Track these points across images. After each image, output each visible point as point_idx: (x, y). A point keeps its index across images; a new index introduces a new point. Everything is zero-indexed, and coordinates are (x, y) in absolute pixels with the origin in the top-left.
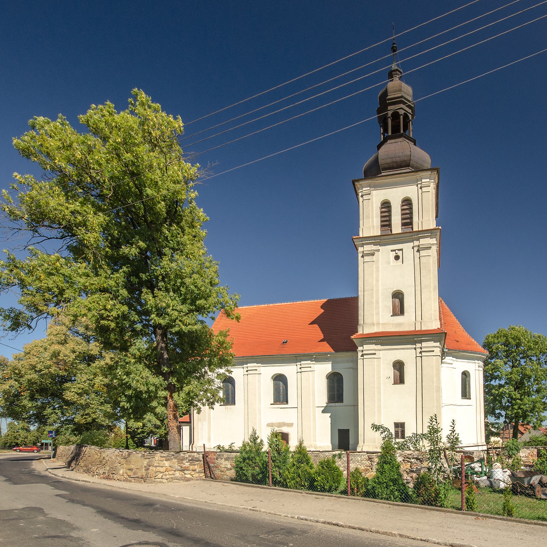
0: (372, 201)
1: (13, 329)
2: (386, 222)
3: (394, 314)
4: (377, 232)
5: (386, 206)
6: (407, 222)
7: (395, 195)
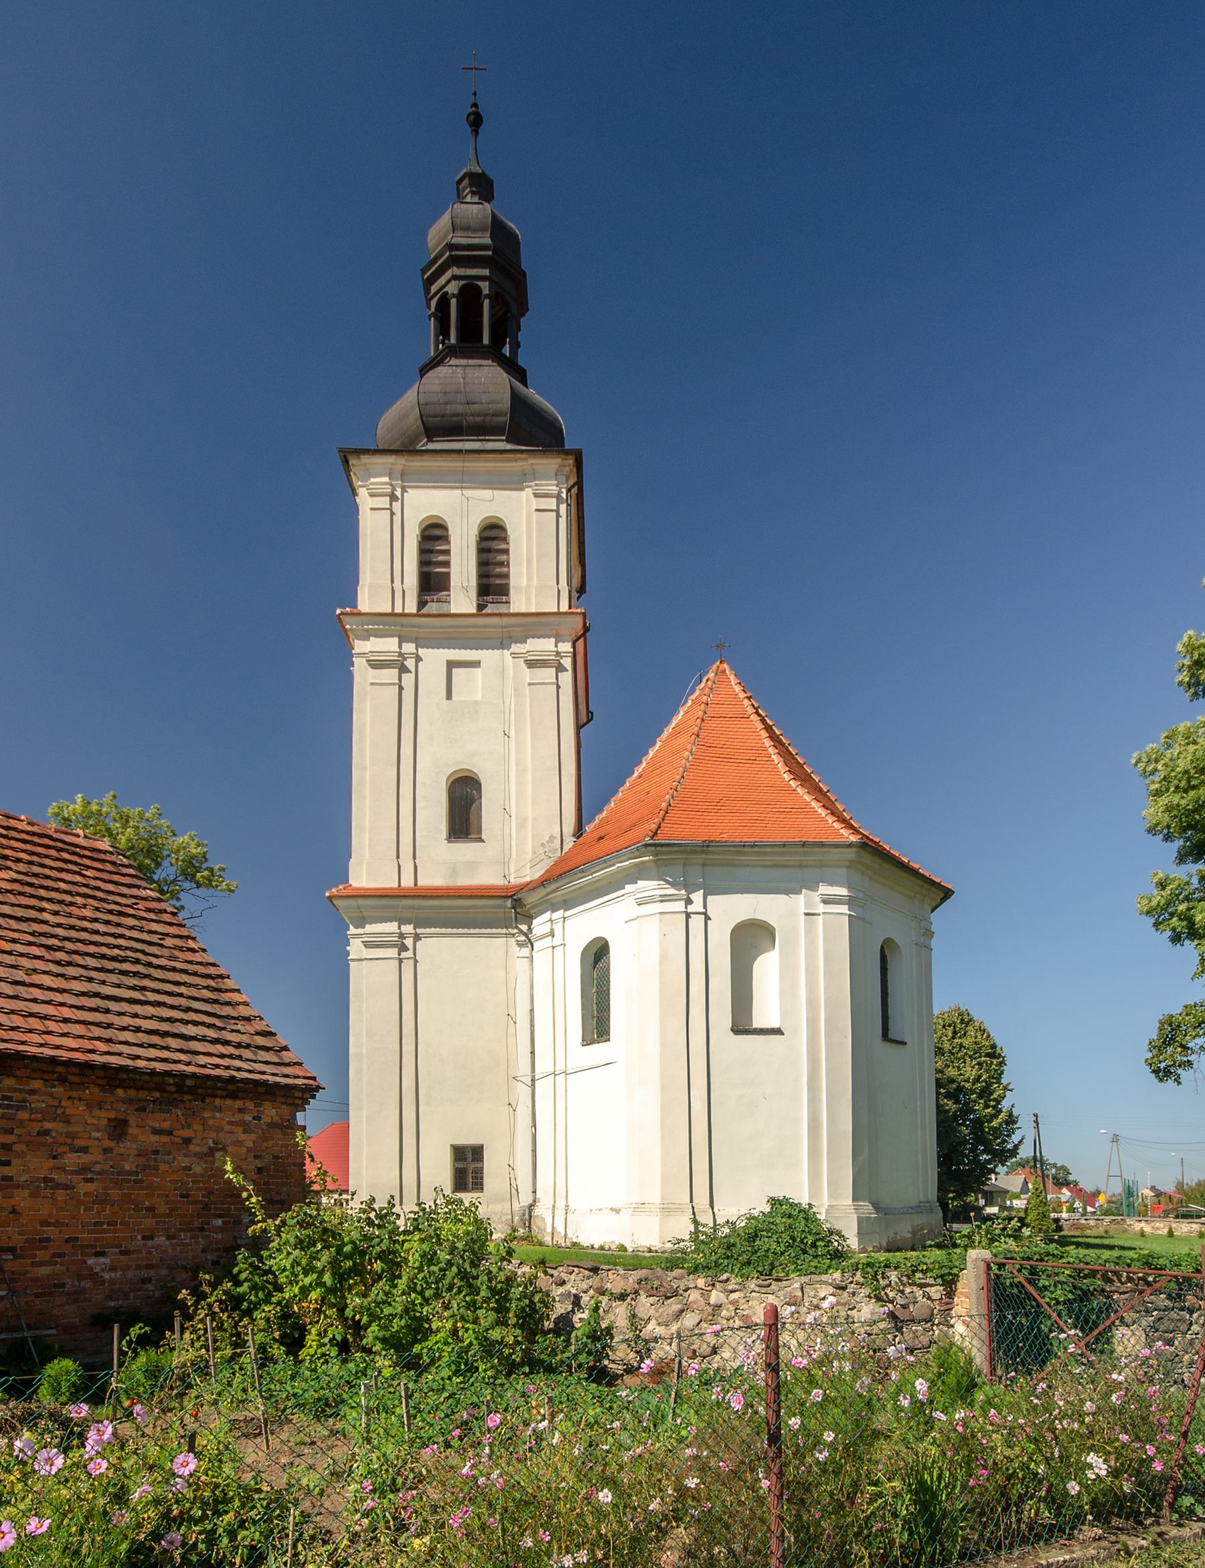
0: (389, 515)
1: (1179, 1183)
2: (432, 582)
3: (587, 1041)
4: (414, 611)
5: (434, 536)
6: (492, 584)
7: (462, 508)
